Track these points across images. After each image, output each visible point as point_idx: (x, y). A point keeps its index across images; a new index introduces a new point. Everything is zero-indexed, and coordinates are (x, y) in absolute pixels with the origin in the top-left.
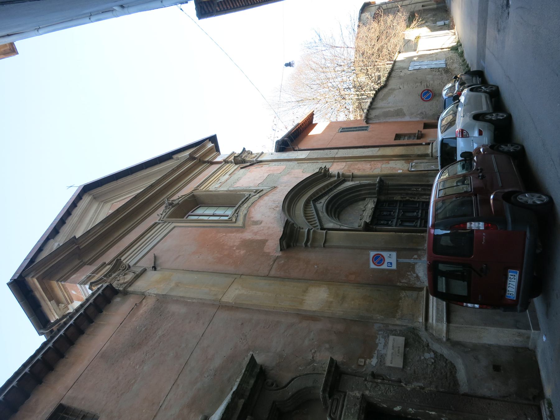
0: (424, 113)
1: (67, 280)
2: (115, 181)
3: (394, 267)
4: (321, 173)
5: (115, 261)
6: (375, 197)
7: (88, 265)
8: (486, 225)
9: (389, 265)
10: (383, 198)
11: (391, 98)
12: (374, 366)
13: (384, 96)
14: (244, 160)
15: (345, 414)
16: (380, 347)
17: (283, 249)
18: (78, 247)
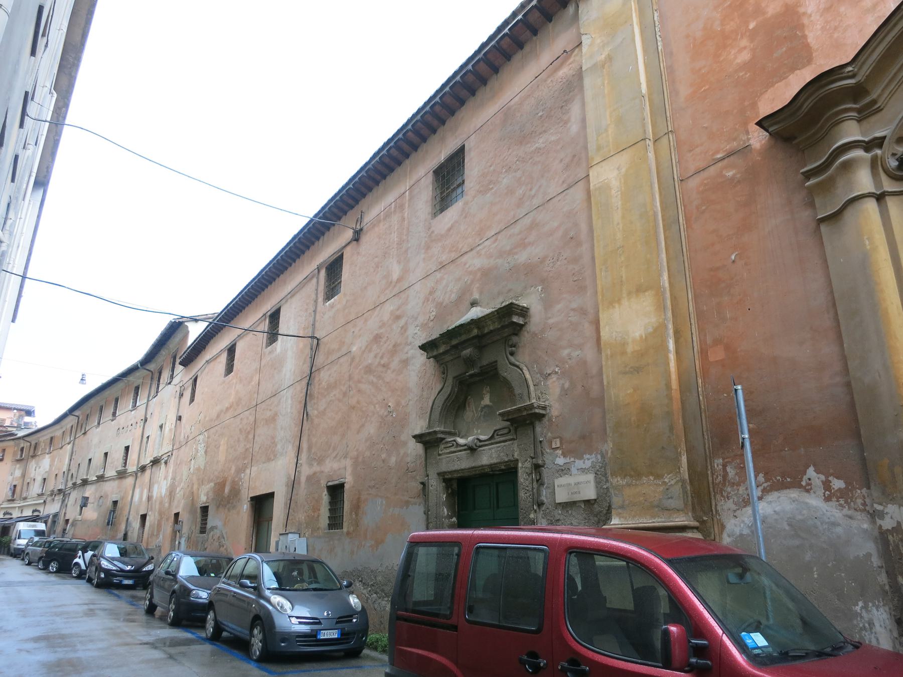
12: (554, 463)
15: (499, 447)
16: (579, 464)
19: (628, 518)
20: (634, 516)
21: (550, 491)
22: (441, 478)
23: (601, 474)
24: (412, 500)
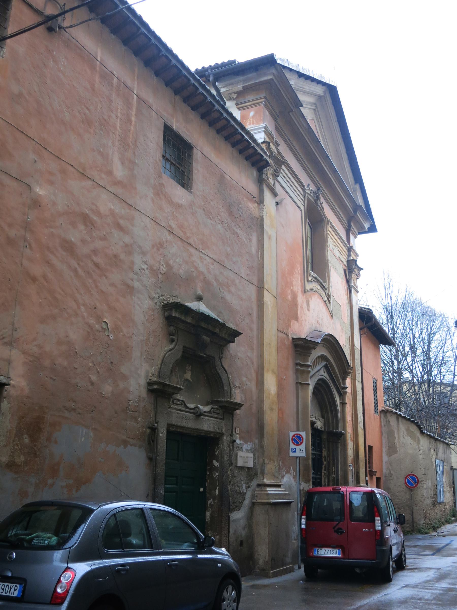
0: (391, 478)
1: (266, 108)
2: (336, 119)
3: (292, 454)
4: (348, 369)
5: (281, 159)
6: (325, 429)
7: (275, 125)
8: (379, 532)
9: (294, 450)
10: (324, 437)
11: (408, 440)
13: (412, 432)
14: (352, 271)
17: (294, 341)
18: (292, 111)
24: (131, 440)
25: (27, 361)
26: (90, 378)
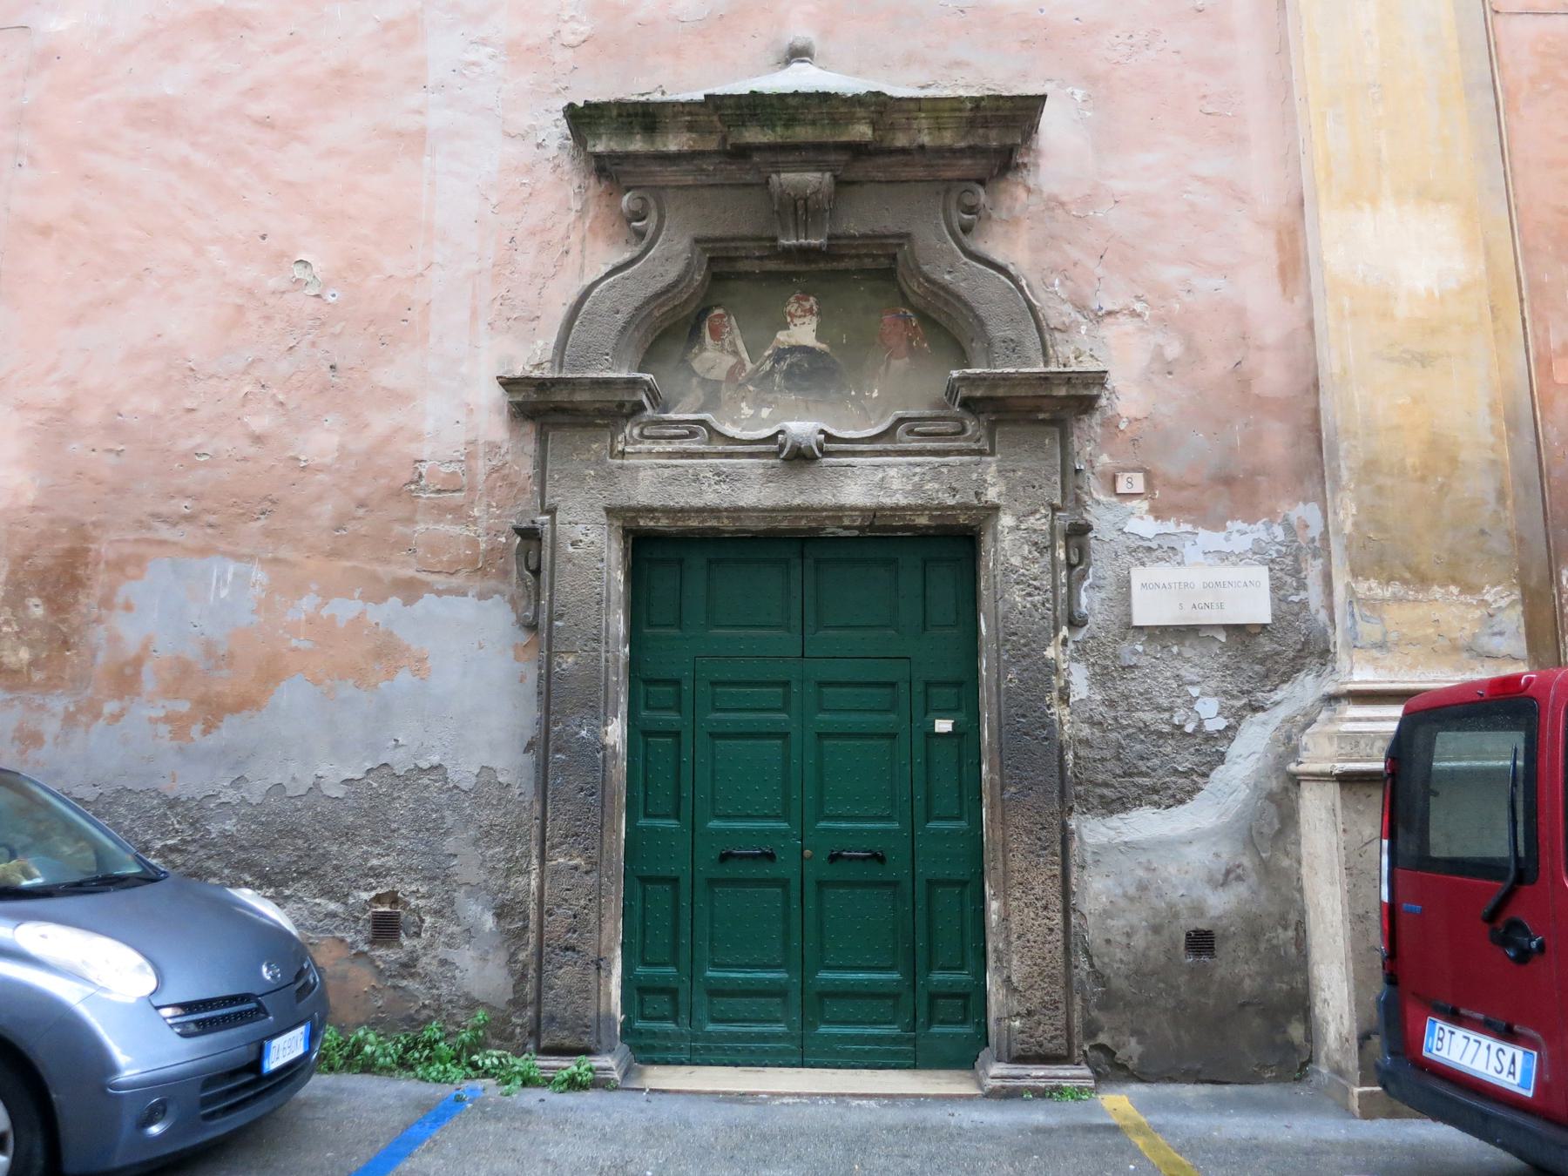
19: (1397, 669)
20: (1412, 667)
21: (1103, 595)
22: (618, 523)
23: (1282, 570)
25: (30, 424)
26: (246, 425)
